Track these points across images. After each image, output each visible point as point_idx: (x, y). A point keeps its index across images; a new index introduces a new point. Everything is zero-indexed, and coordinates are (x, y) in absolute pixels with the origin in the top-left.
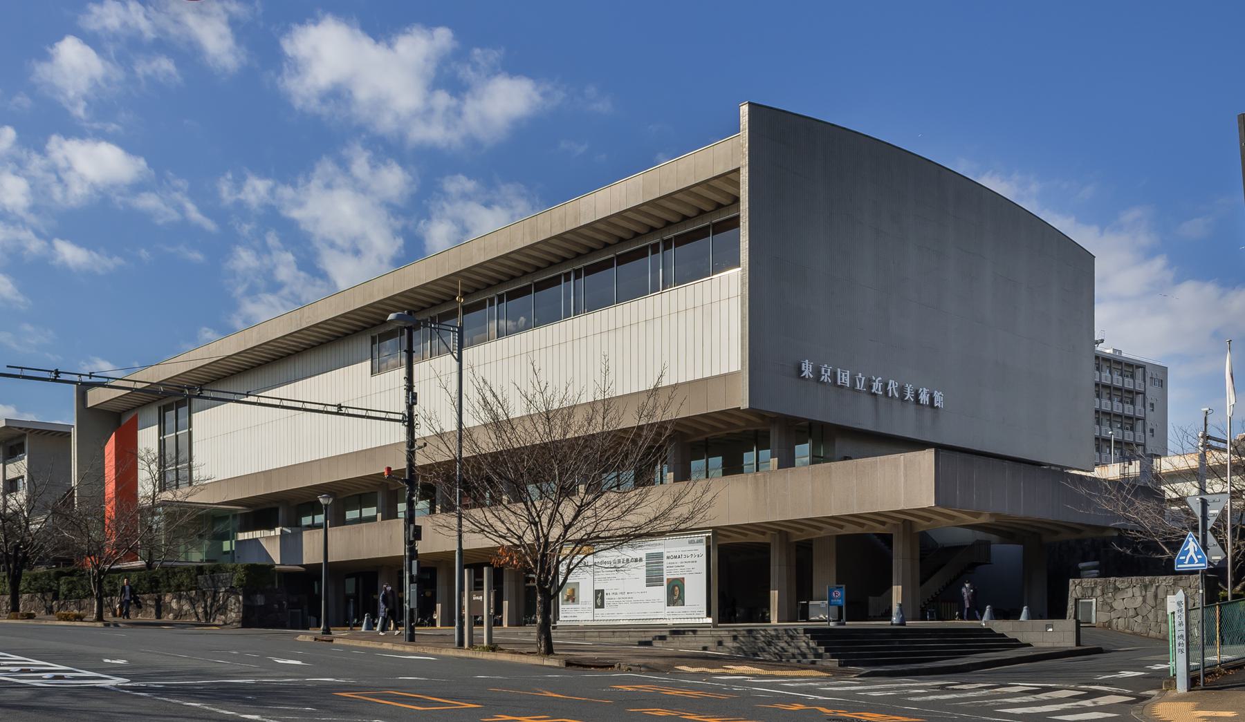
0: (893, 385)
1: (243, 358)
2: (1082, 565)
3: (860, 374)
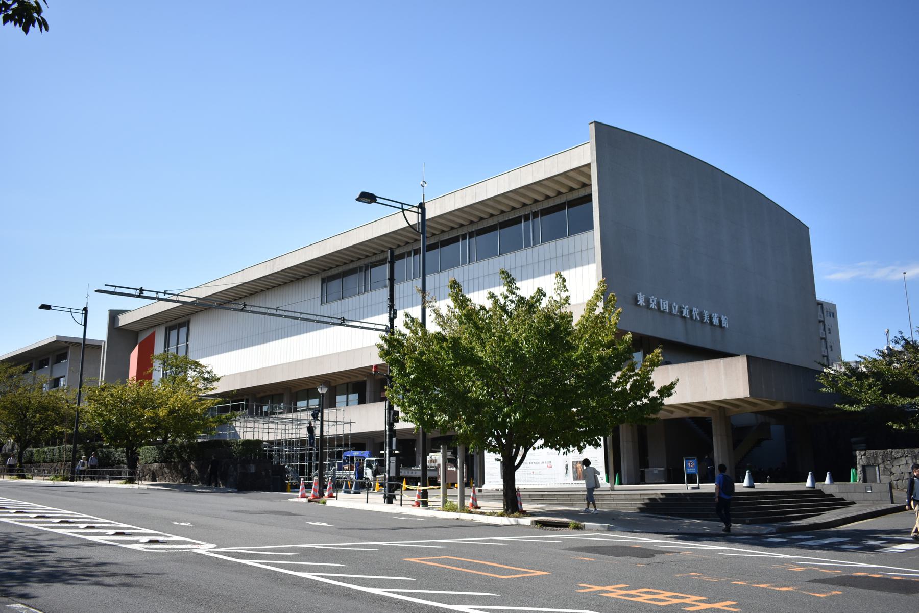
0: (696, 312)
1: (229, 293)
2: (853, 440)
3: (675, 303)
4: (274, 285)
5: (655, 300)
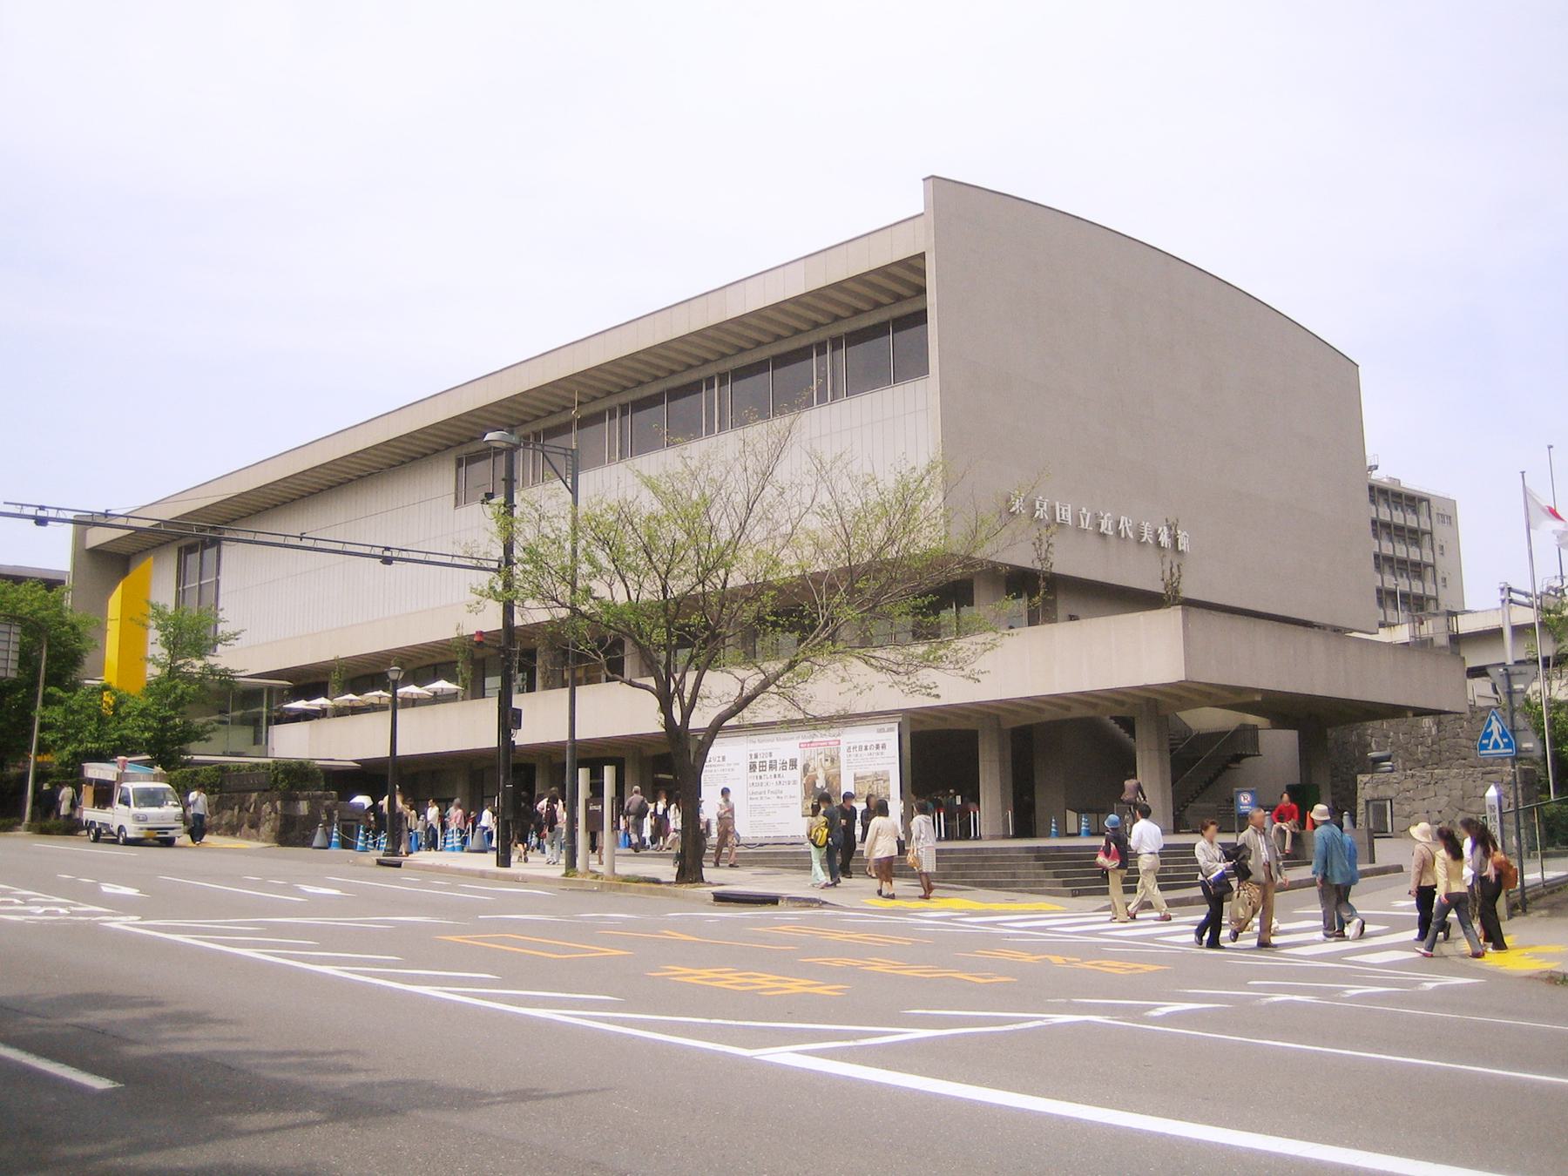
4: (449, 443)
5: (1045, 504)
